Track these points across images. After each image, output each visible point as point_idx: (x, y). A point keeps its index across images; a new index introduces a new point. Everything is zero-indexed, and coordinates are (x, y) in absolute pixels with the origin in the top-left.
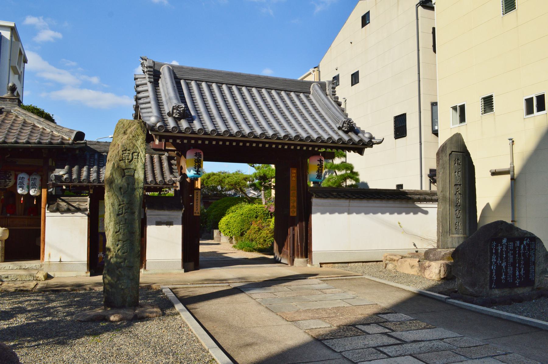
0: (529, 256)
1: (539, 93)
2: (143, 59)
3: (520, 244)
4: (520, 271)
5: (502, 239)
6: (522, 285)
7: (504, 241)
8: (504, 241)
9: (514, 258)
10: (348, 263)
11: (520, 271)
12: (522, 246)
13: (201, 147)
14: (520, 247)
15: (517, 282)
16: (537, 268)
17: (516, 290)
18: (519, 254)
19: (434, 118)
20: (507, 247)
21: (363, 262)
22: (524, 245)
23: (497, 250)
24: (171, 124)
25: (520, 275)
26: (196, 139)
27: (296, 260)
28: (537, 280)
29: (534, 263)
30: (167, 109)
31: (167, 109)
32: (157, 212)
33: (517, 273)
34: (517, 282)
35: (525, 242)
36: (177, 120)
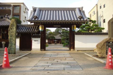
1: (80, 6)
7: (111, 42)
8: (111, 42)
23: (108, 45)
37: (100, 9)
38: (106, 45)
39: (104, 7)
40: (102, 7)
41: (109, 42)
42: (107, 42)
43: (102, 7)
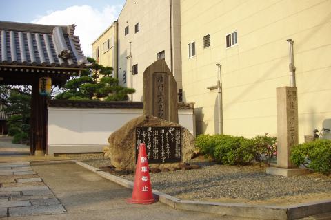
0: (175, 140)
1: (233, 31)
2: (137, 26)
3: (165, 132)
4: (165, 151)
5: (147, 127)
6: (167, 161)
7: (149, 129)
8: (149, 129)
9: (160, 142)
10: (81, 153)
11: (165, 151)
12: (167, 134)
13: (51, 75)
14: (165, 134)
15: (163, 159)
16: (183, 150)
17: (162, 165)
18: (165, 139)
19: (179, 50)
20: (152, 133)
21: (94, 153)
22: (169, 133)
23: (141, 136)
24: (61, 61)
25: (166, 154)
26: (51, 70)
27: (37, 152)
28: (184, 158)
29: (180, 146)
30: (58, 53)
31: (58, 53)
32: (64, 131)
33: (163, 153)
34: (163, 159)
35: (170, 131)
36: (65, 60)
37: (126, 34)
38: (137, 136)
39: (137, 30)
40: (132, 30)
41: (145, 129)
42: (137, 128)
43: (132, 30)
